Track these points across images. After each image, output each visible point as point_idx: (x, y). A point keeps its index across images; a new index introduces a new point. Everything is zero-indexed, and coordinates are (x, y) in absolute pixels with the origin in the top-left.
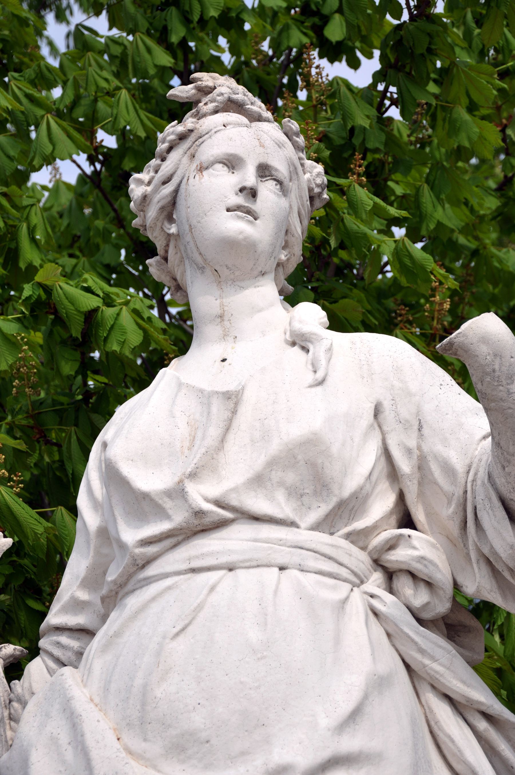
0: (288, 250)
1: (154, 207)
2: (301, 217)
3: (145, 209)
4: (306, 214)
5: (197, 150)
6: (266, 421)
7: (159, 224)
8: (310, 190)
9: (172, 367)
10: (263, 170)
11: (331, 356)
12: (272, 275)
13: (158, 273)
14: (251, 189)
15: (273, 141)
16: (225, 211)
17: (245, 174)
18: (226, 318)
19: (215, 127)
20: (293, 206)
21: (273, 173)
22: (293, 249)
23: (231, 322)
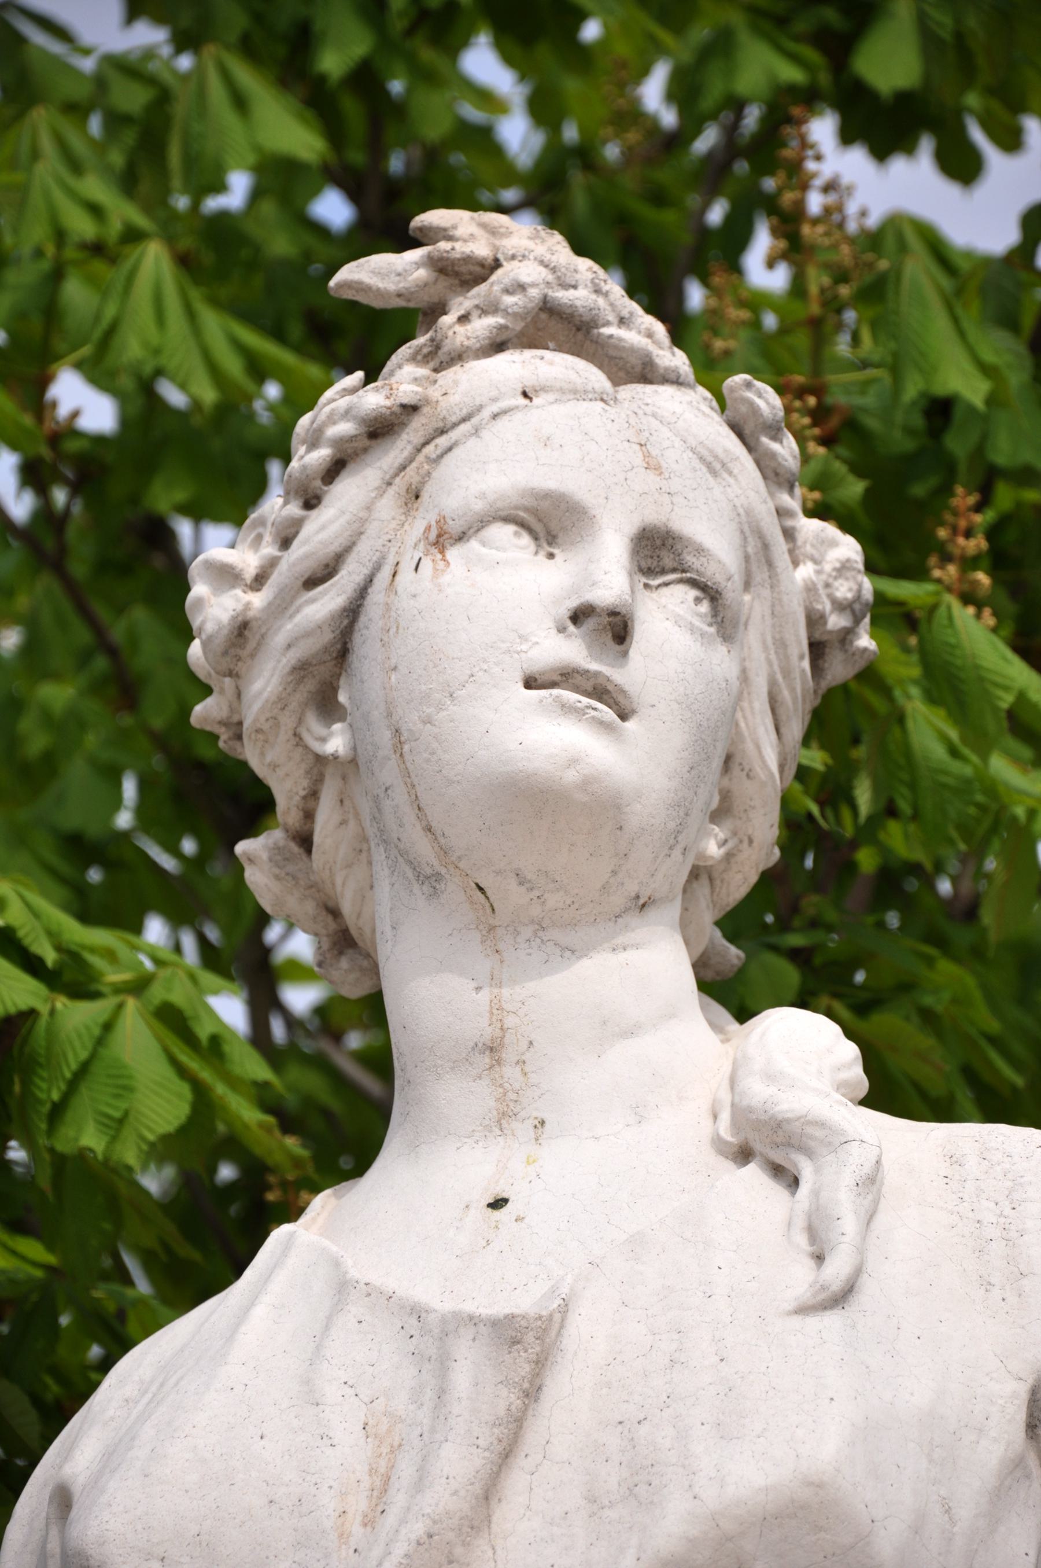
0: (729, 823)
1: (270, 665)
2: (781, 711)
3: (241, 668)
4: (795, 700)
5: (429, 474)
6: (644, 1430)
7: (288, 721)
8: (814, 620)
9: (314, 1219)
10: (655, 548)
11: (876, 1203)
12: (675, 910)
13: (276, 887)
14: (613, 613)
15: (693, 450)
16: (521, 685)
17: (590, 561)
18: (509, 1055)
19: (494, 400)
20: (751, 674)
21: (690, 559)
22: (749, 820)
23: (527, 1068)
